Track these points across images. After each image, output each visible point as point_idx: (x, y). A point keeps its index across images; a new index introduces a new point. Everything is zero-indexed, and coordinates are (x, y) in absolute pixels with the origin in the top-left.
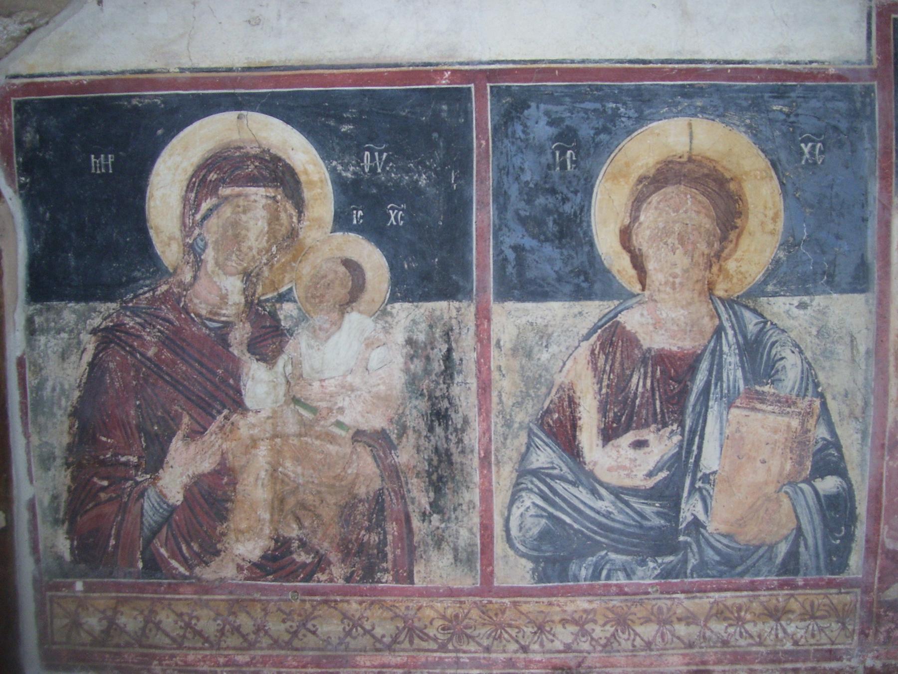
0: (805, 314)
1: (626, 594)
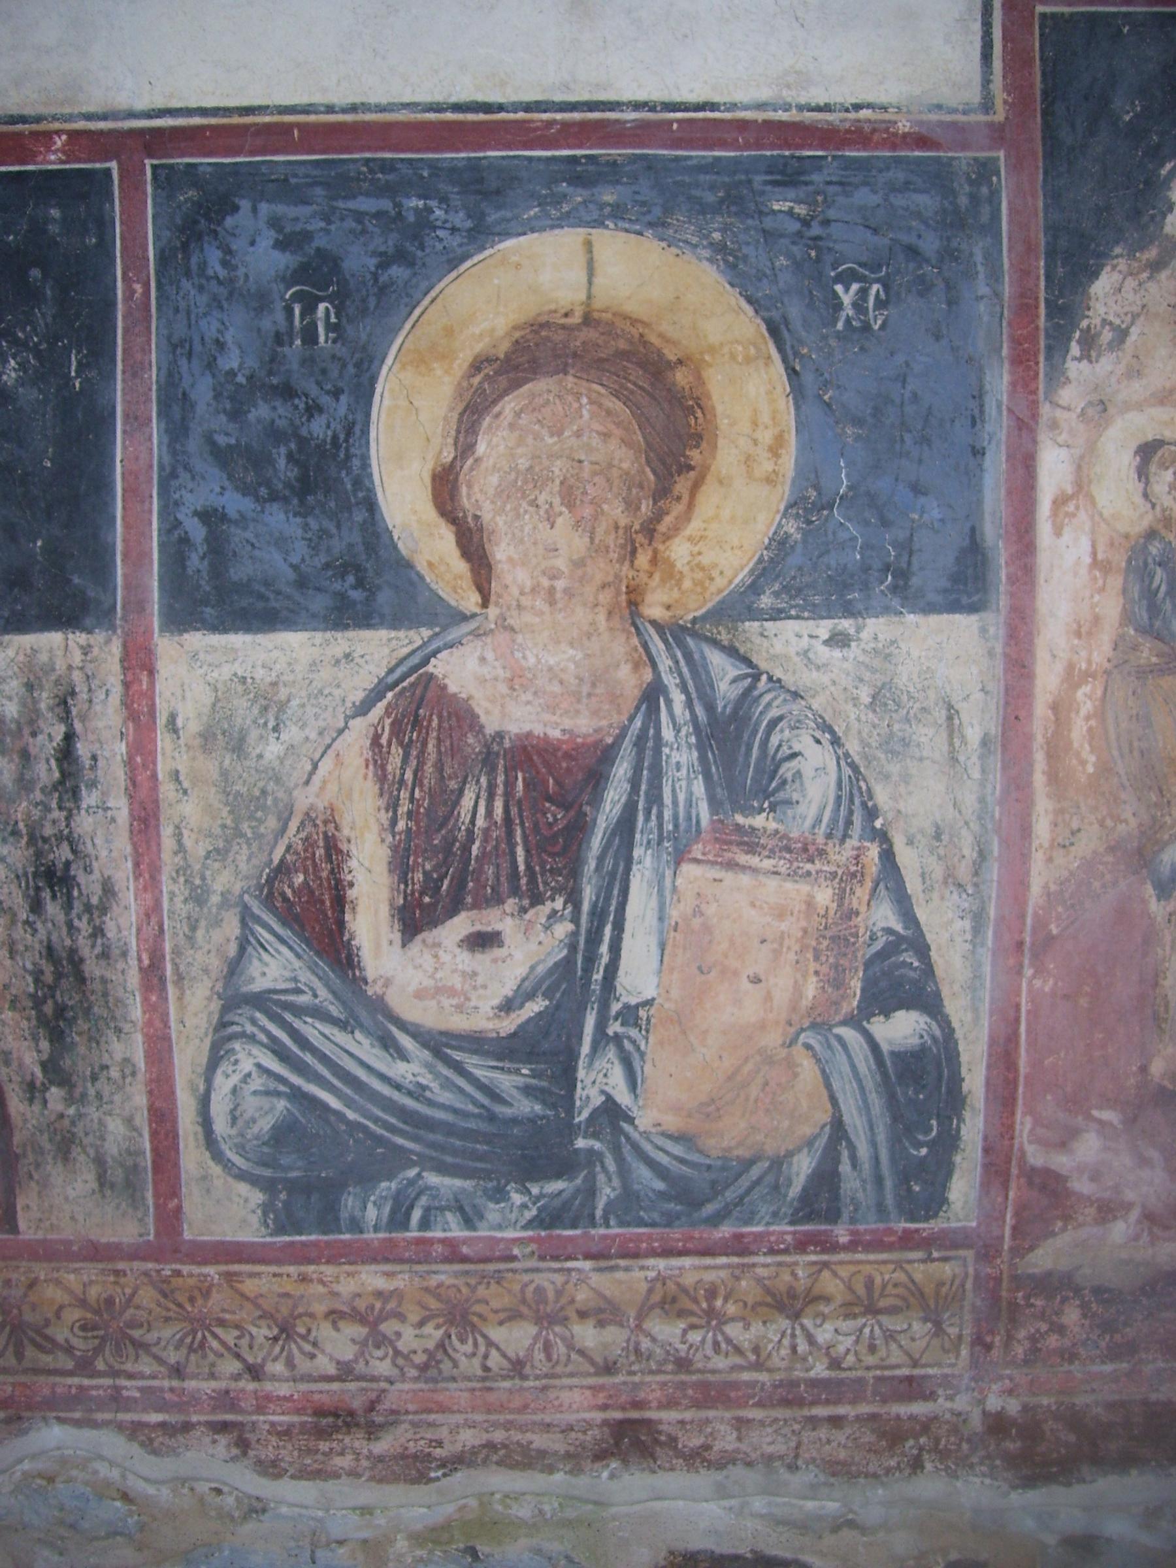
0: (845, 659)
1: (465, 1259)
